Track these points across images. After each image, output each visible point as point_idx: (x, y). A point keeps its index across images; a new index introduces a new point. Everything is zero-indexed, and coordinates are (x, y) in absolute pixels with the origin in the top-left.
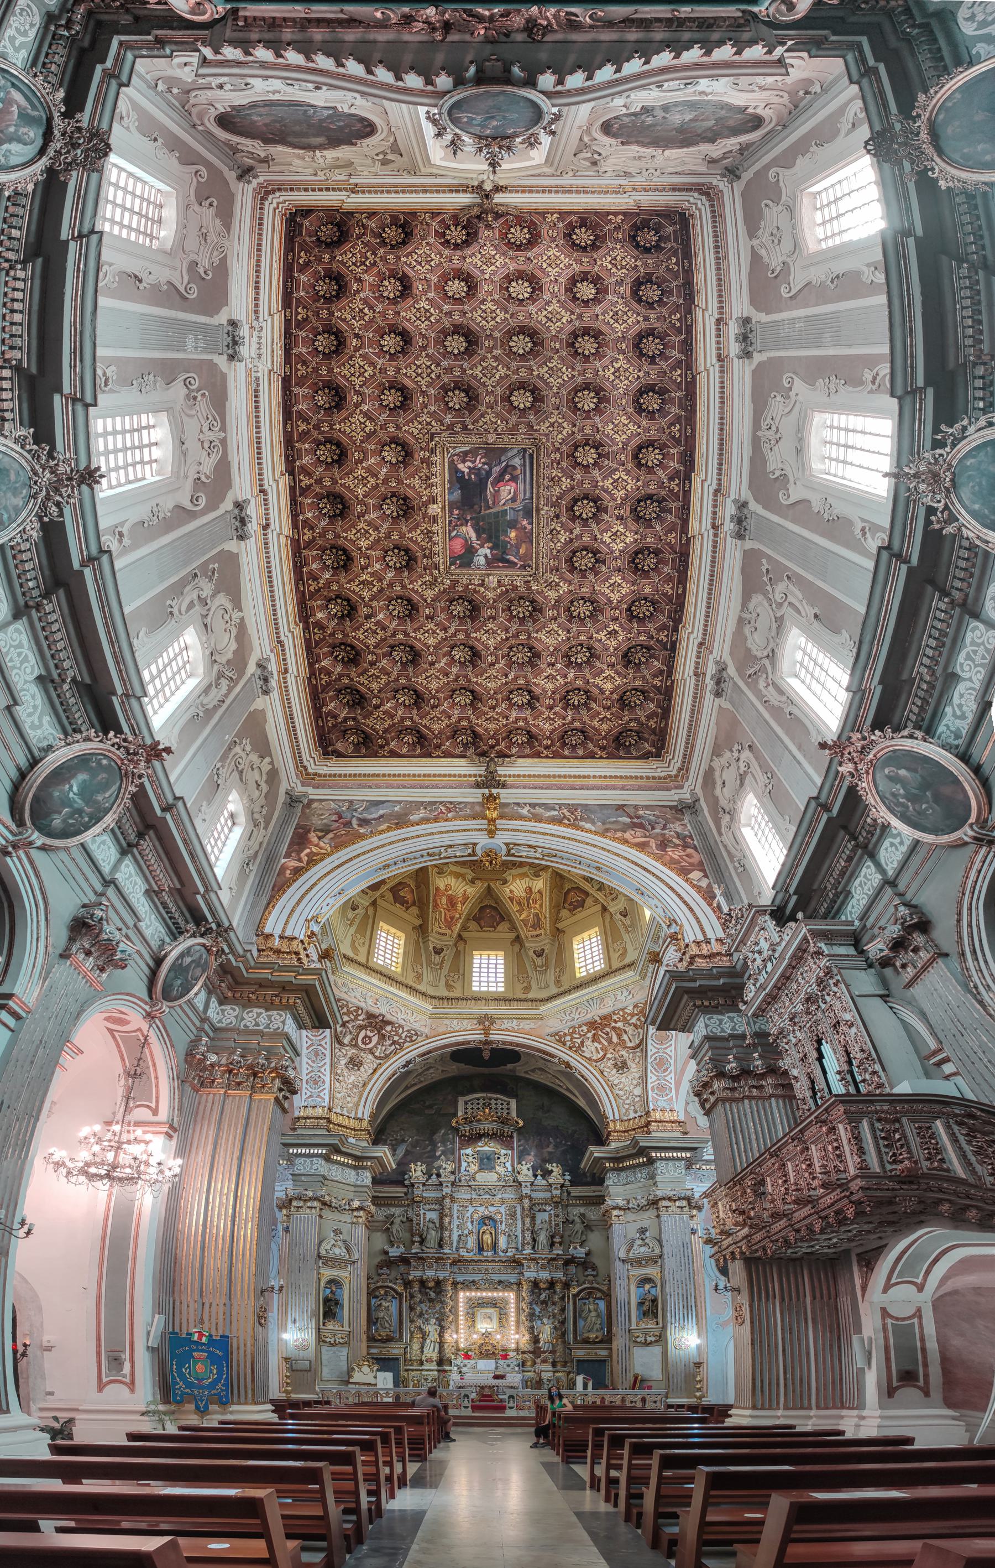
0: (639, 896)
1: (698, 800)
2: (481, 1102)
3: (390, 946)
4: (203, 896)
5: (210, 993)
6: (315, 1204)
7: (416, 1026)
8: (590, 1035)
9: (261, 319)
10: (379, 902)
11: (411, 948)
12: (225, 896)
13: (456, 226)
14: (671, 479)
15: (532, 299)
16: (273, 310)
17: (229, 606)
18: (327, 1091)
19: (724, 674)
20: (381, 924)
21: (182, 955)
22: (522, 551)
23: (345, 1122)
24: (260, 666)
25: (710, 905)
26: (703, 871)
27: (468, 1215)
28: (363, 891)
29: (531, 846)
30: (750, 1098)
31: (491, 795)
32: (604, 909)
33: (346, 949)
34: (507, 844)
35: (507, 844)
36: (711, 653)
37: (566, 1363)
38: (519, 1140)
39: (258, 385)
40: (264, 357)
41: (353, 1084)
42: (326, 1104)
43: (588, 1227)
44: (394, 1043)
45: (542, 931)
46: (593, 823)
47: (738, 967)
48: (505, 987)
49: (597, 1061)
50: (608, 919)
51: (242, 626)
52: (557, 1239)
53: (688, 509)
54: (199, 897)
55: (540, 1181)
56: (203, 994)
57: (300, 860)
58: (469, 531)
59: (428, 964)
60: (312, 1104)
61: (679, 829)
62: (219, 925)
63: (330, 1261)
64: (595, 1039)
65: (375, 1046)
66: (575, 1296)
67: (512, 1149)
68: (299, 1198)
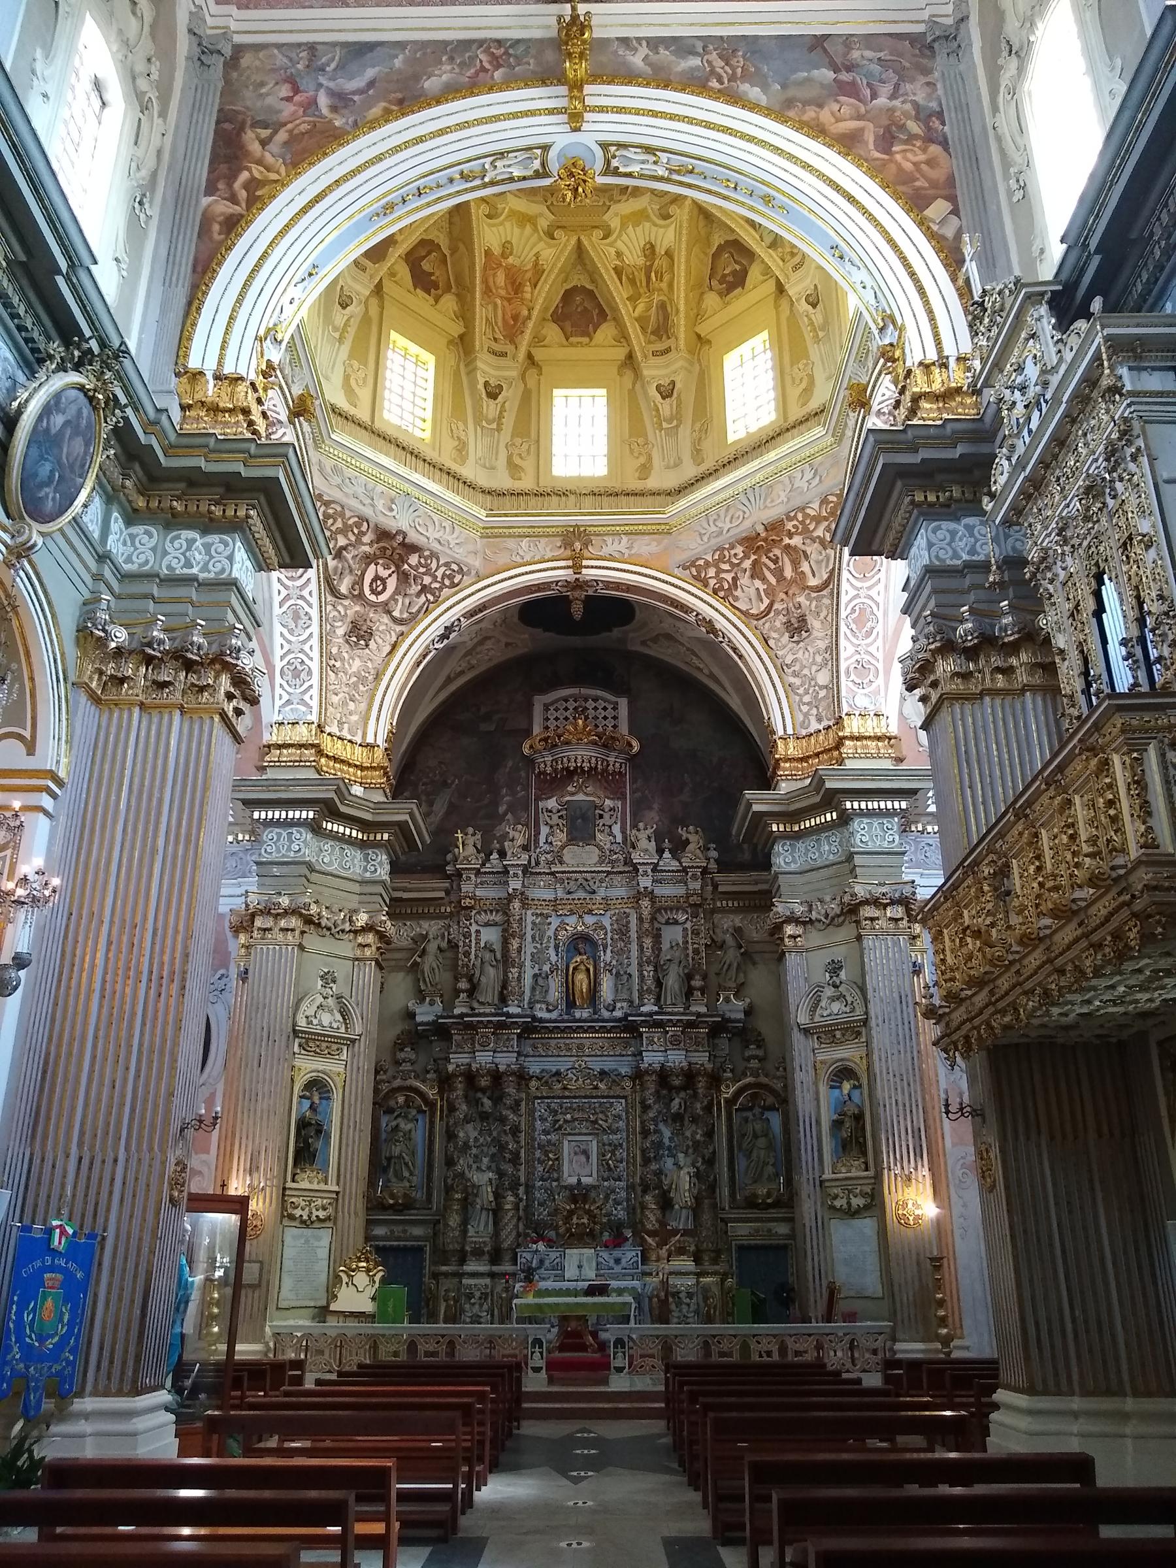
0: (835, 262)
1: (963, 19)
2: (571, 705)
3: (410, 383)
4: (68, 279)
5: (109, 500)
6: (294, 922)
7: (460, 554)
8: (747, 564)
10: (388, 286)
11: (448, 388)
12: (107, 277)
18: (315, 692)
20: (394, 335)
21: (47, 411)
23: (345, 752)
25: (954, 280)
26: (952, 199)
27: (550, 933)
28: (356, 263)
29: (649, 150)
30: (994, 692)
31: (575, 17)
32: (780, 289)
33: (335, 395)
34: (604, 146)
37: (718, 1252)
38: (634, 780)
41: (357, 675)
42: (314, 718)
43: (748, 957)
44: (425, 589)
45: (671, 342)
46: (765, 87)
47: (988, 419)
49: (758, 617)
52: (697, 983)
54: (60, 281)
55: (668, 862)
56: (97, 503)
57: (233, 199)
59: (477, 422)
60: (291, 717)
61: (920, 98)
62: (103, 344)
63: (313, 1042)
64: (756, 573)
65: (392, 598)
66: (730, 1102)
67: (623, 797)
68: (266, 912)
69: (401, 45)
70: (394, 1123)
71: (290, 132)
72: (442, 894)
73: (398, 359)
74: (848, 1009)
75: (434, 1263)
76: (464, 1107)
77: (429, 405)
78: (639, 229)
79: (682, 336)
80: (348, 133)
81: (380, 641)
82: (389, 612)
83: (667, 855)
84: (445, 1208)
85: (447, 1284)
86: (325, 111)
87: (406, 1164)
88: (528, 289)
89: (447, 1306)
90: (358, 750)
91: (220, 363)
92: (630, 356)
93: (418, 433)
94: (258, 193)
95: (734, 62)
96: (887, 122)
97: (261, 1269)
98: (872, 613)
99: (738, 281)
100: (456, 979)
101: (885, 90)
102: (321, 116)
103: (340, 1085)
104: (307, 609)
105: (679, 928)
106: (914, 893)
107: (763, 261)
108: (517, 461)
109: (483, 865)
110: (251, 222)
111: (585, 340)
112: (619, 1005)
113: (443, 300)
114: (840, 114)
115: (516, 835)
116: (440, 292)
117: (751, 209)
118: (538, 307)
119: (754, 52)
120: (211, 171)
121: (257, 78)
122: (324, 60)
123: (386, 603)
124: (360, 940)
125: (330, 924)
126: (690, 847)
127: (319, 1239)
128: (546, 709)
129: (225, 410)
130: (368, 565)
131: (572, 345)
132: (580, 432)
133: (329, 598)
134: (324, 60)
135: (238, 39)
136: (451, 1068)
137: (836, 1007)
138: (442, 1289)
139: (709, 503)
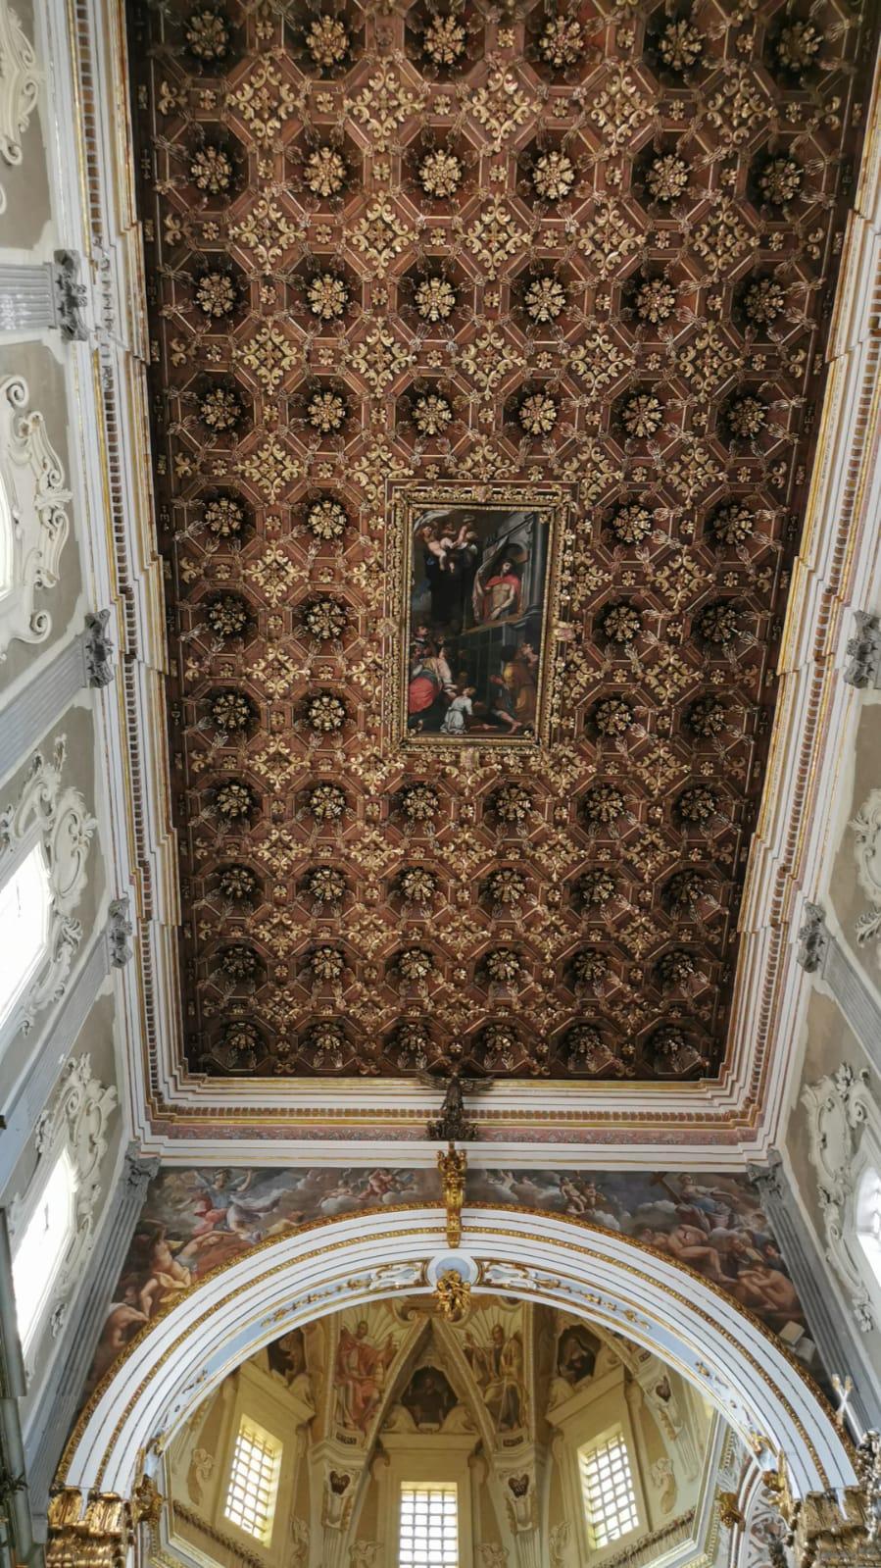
1: (779, 1165)
9: (105, 243)
13: (445, 15)
14: (760, 567)
15: (574, 152)
16: (125, 223)
17: (79, 809)
19: (821, 930)
20: (245, 1420)
22: (520, 703)
24: (115, 914)
25: (833, 1421)
29: (519, 1266)
31: (452, 1154)
32: (629, 1379)
34: (479, 1261)
35: (479, 1261)
36: (799, 886)
39: (110, 384)
40: (116, 325)
46: (617, 1214)
50: (635, 1393)
51: (94, 844)
53: (781, 625)
57: (138, 1306)
58: (441, 667)
61: (754, 1227)
69: (304, 1171)
73: (246, 1446)
78: (488, 1312)
79: (533, 1424)
80: (251, 1246)
86: (233, 1226)
88: (380, 1370)
91: (99, 1481)
92: (480, 1445)
93: (257, 1534)
94: (163, 1300)
95: (588, 1192)
99: (583, 1369)
101: (722, 1220)
107: (609, 1349)
110: (153, 1329)
111: (435, 1426)
113: (296, 1382)
114: (683, 1237)
116: (294, 1372)
117: (615, 1322)
118: (388, 1391)
119: (603, 1185)
120: (122, 1278)
121: (176, 1195)
122: (236, 1182)
131: (422, 1432)
134: (236, 1182)
135: (165, 1163)
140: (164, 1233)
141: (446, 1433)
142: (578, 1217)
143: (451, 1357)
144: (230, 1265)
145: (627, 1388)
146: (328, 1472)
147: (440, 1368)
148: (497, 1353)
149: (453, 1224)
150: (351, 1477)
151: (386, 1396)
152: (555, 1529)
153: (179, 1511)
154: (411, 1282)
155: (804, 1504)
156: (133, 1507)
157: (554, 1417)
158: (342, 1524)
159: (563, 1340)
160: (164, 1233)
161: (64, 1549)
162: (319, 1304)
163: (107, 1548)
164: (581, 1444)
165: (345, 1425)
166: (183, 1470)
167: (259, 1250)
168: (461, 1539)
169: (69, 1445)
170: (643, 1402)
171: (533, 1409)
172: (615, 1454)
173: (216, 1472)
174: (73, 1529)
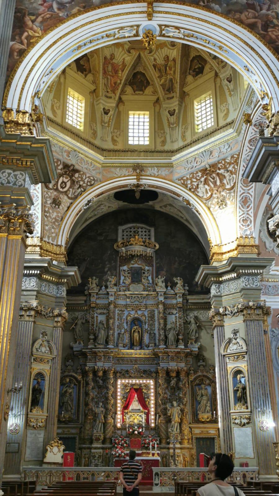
8: (203, 179)
27: (124, 317)
29: (177, 28)
32: (216, 75)
34: (160, 26)
35: (160, 26)
38: (157, 259)
41: (55, 218)
45: (174, 94)
46: (220, 5)
48: (150, 141)
52: (180, 337)
57: (22, 43)
64: (206, 182)
65: (68, 190)
67: (152, 266)
70: (65, 389)
71: (43, 17)
72: (83, 302)
73: (71, 98)
74: (240, 348)
75: (80, 444)
76: (92, 383)
77: (83, 117)
78: (163, 50)
79: (178, 92)
80: (65, 19)
81: (63, 206)
82: (67, 195)
83: (169, 288)
84: (85, 422)
85: (85, 451)
86: (56, 10)
87: (69, 405)
88: (120, 72)
89: (85, 460)
90: (55, 247)
91: (19, 106)
92: (158, 99)
93: (78, 127)
94: (31, 41)
96: (266, 20)
97: (19, 446)
98: (250, 199)
99: (199, 71)
100: (89, 335)
102: (54, 12)
103: (48, 375)
104: (37, 194)
105: (174, 316)
106: (265, 305)
107: (210, 64)
108: (115, 138)
109: (99, 291)
110: (29, 52)
111: (141, 92)
112: (151, 345)
113: (88, 76)
114: (248, 15)
115: (112, 280)
116: (87, 73)
117: (214, 51)
120: (13, 32)
123: (66, 192)
124: (56, 319)
125: (45, 314)
126: (178, 285)
127: (40, 434)
128: (123, 231)
129: (21, 124)
130: (60, 177)
131: (136, 94)
132: (139, 128)
133: (46, 190)
136: (87, 368)
137: (235, 347)
138: (83, 454)
139: (188, 156)
140: (27, 13)
141: (145, 95)
142: (204, 6)
143: (148, 68)
144: (57, 27)
145: (215, 78)
146: (102, 107)
147: (143, 72)
148: (166, 66)
149: (150, 10)
150: (111, 110)
151: (123, 82)
152: (184, 127)
153: (49, 119)
154: (132, 35)
155: (276, 115)
156: (33, 115)
157: (186, 89)
158: (108, 125)
159: (192, 61)
160: (27, 13)
161: (11, 127)
162: (95, 44)
163: (26, 127)
164: (196, 98)
165: (108, 92)
166: (49, 106)
167: (68, 20)
168: (150, 129)
169: (5, 94)
170: (221, 84)
171: (178, 87)
172: (208, 102)
173: (61, 107)
174: (13, 121)
